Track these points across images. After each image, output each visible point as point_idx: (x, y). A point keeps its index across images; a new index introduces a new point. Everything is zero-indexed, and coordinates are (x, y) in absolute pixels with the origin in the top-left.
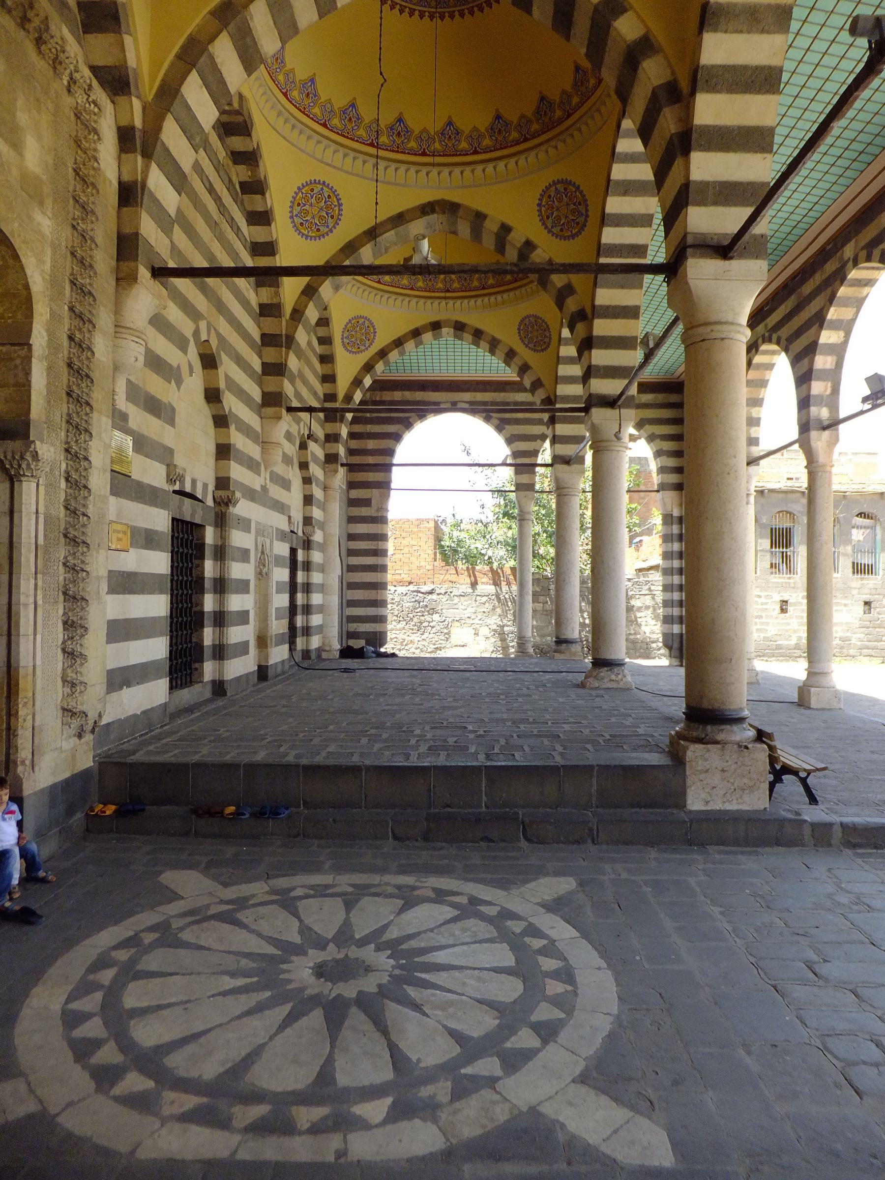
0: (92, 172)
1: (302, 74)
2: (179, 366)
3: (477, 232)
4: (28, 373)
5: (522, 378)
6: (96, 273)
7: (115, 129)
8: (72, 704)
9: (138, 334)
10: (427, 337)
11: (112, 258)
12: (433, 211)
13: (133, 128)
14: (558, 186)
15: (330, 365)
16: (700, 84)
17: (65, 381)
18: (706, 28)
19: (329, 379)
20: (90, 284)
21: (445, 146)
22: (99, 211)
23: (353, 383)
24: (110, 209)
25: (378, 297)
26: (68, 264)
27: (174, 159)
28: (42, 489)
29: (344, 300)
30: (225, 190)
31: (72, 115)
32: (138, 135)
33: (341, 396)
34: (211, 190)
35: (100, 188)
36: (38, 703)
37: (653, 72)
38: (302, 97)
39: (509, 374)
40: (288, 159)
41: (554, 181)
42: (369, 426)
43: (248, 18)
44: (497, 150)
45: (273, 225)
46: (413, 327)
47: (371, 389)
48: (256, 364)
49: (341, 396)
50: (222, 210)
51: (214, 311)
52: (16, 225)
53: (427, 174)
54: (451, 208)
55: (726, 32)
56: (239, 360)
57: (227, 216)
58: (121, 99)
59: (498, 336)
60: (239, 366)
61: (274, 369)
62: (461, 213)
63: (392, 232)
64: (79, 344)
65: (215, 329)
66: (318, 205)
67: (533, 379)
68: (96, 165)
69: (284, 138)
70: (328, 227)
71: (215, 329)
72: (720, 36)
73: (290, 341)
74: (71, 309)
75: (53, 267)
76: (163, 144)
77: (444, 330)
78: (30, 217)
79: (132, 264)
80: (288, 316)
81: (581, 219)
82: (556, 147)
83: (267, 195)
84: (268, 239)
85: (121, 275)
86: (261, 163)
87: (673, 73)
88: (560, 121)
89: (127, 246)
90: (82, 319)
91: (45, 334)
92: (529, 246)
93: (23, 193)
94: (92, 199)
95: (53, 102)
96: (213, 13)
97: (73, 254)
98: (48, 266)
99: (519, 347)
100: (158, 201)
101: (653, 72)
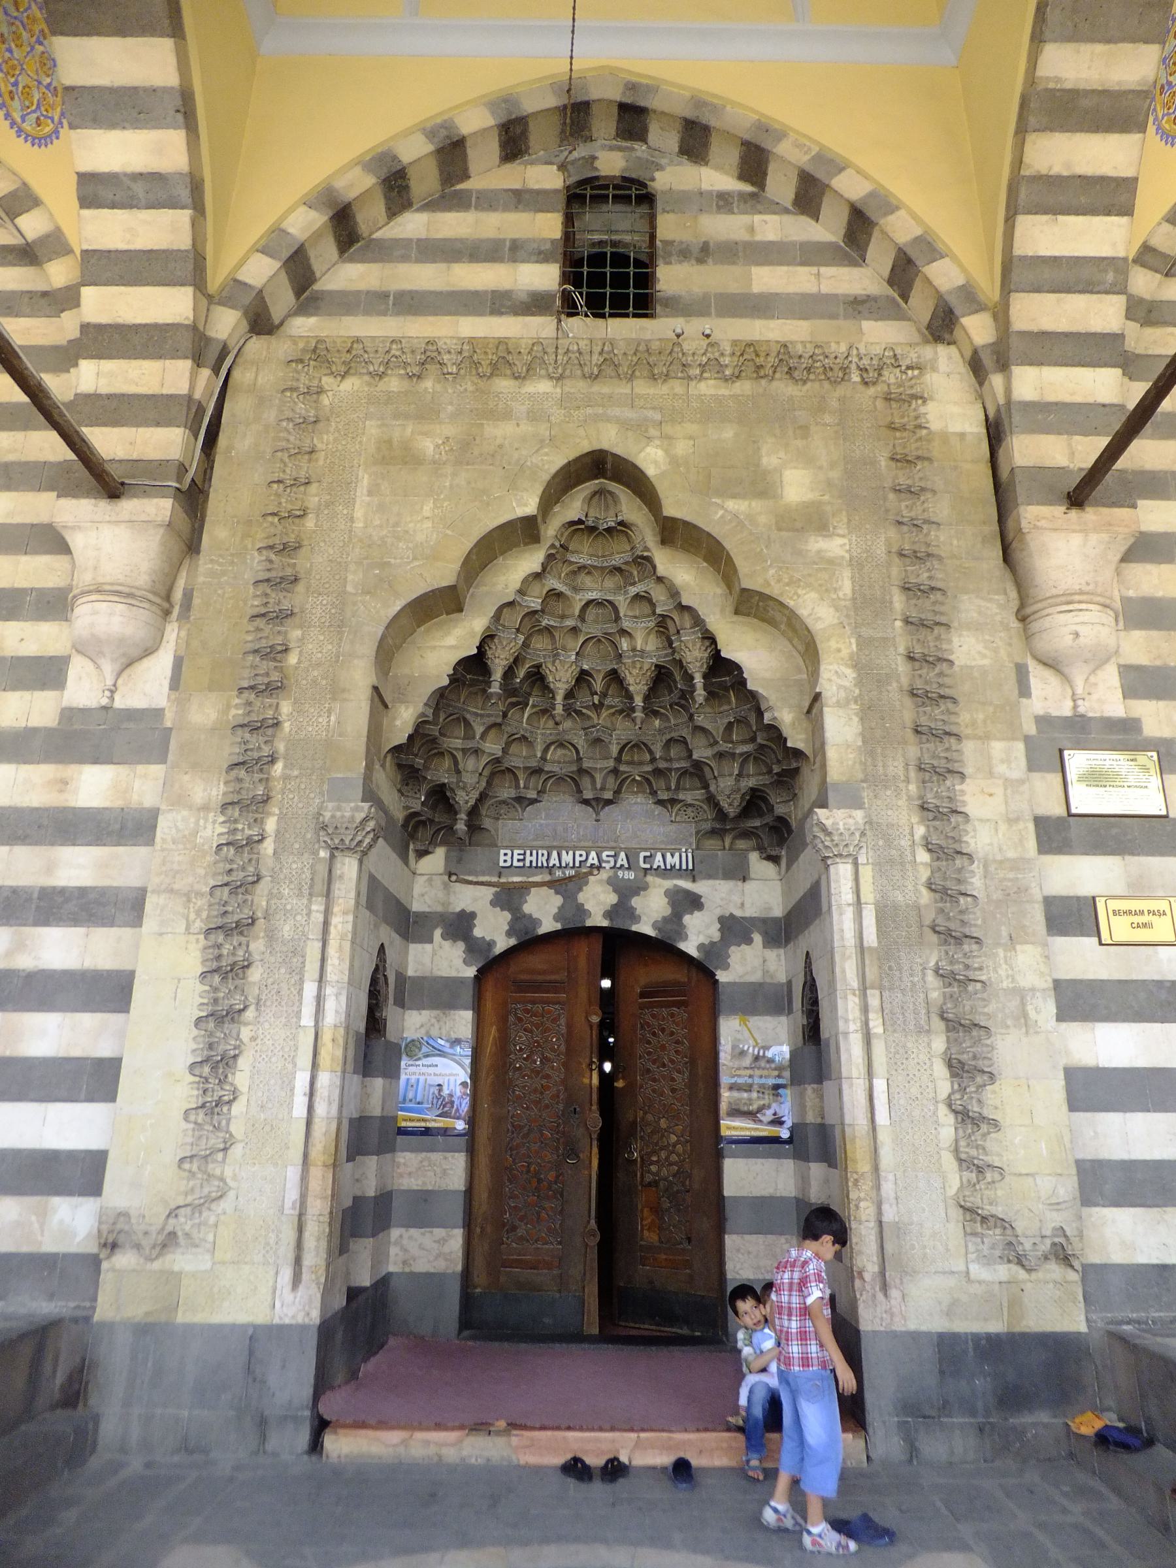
8: (974, 1200)
9: (1063, 599)
20: (930, 578)
28: (866, 873)
36: (888, 1188)
43: (1051, 85)
68: (924, 432)
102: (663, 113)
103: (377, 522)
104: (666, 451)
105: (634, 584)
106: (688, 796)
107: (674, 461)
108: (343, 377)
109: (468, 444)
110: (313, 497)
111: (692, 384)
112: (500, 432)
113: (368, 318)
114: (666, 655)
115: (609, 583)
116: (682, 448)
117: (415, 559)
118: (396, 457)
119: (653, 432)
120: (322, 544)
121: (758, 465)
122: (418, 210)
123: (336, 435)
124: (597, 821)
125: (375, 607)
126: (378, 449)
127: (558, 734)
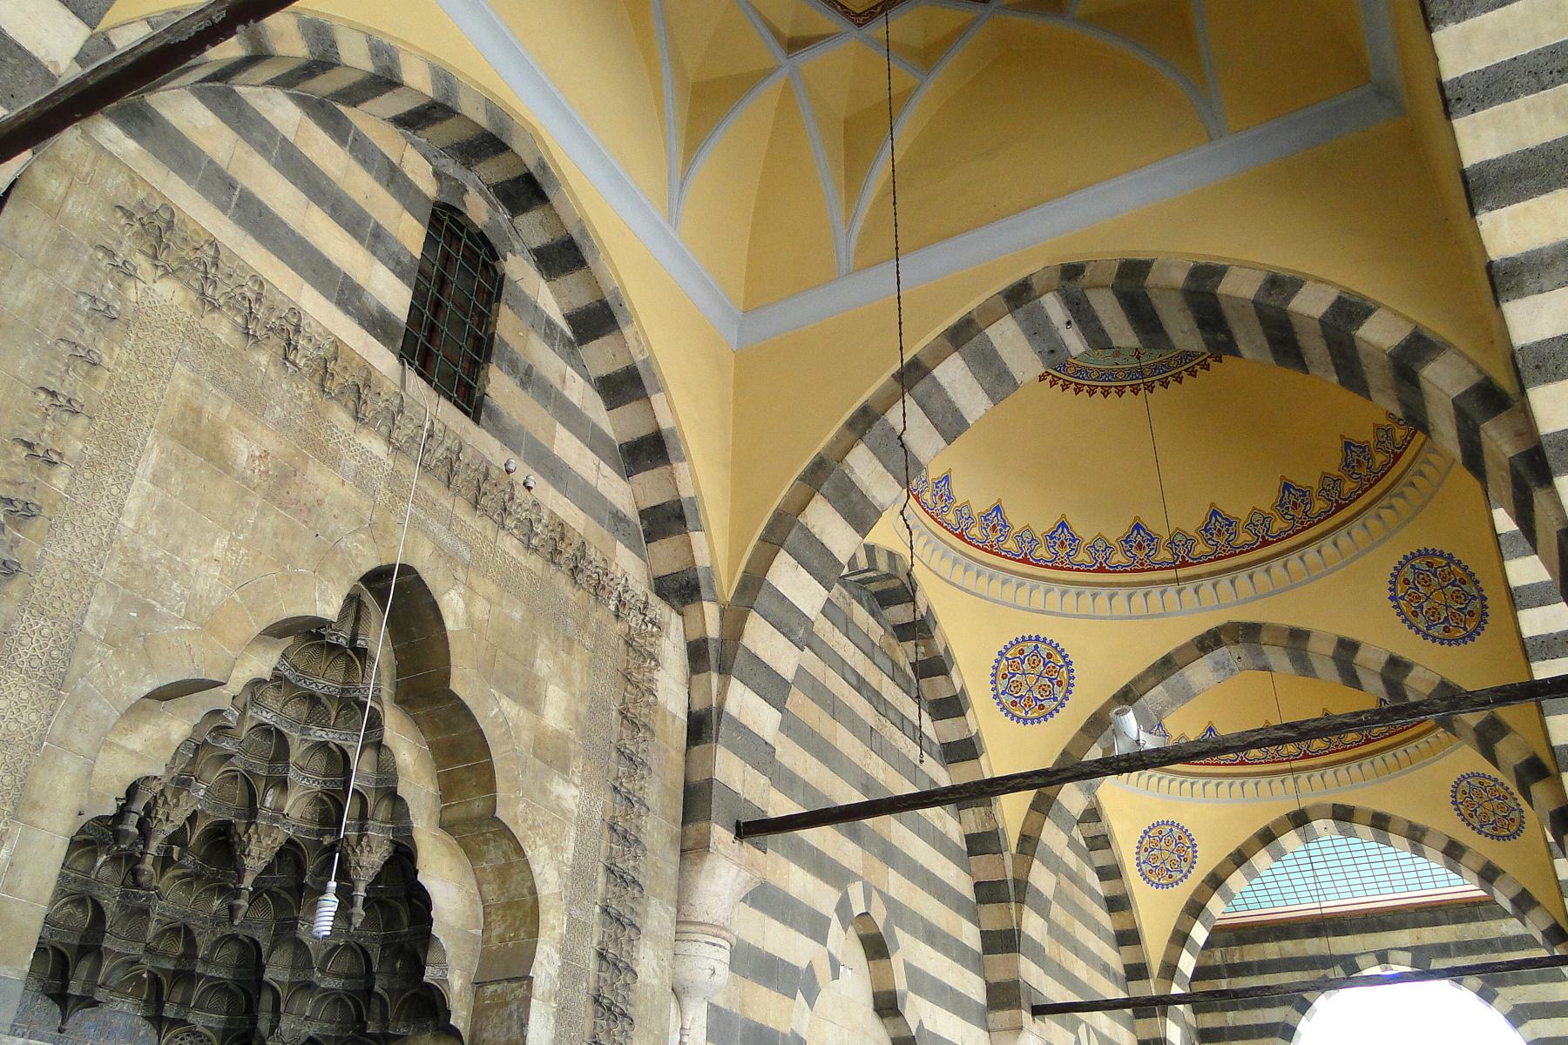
0: (645, 711)
1: (980, 505)
2: (810, 966)
3: (1302, 664)
4: (523, 1024)
5: (1490, 892)
6: (644, 850)
7: (683, 647)
9: (715, 931)
10: (1290, 840)
11: (675, 821)
12: (1218, 643)
13: (705, 640)
14: (1416, 562)
15: (1126, 913)
16: (1526, 375)
17: (588, 1026)
18: (1501, 295)
19: (1128, 937)
21: (1222, 543)
22: (652, 760)
23: (1172, 940)
24: (673, 753)
25: (1187, 785)
26: (604, 844)
27: (767, 667)
29: (1128, 804)
30: (886, 680)
31: (621, 642)
32: (712, 647)
33: (1155, 967)
34: (861, 685)
35: (656, 728)
37: (1444, 380)
38: (988, 535)
39: (1461, 886)
40: (975, 621)
41: (1405, 557)
42: (1230, 1014)
44: (1299, 532)
45: (969, 713)
46: (1259, 826)
47: (1208, 944)
48: (970, 936)
49: (1155, 967)
50: (882, 709)
51: (877, 864)
52: (522, 806)
53: (1196, 591)
54: (1248, 633)
55: (1540, 292)
56: (933, 936)
57: (892, 716)
58: (691, 609)
59: (1419, 820)
60: (932, 944)
61: (1003, 941)
62: (1264, 637)
63: (1160, 688)
64: (615, 963)
65: (880, 892)
66: (1035, 674)
67: (1514, 891)
69: (967, 591)
70: (1055, 699)
71: (880, 892)
72: (1530, 300)
73: (1021, 891)
74: (605, 910)
75: (578, 853)
76: (747, 650)
77: (1319, 825)
78: (544, 791)
79: (703, 825)
80: (1014, 850)
81: (1475, 605)
82: (1391, 507)
83: (953, 673)
84: (966, 735)
85: (690, 844)
86: (937, 633)
87: (1480, 371)
88: (1387, 468)
89: (696, 799)
90: (620, 923)
91: (556, 957)
92: (1396, 667)
93: (538, 761)
94: (643, 746)
95: (591, 635)
96: (801, 479)
97: (612, 828)
98: (569, 855)
99: (1465, 835)
100: (745, 727)
101: (1444, 380)
102: (557, 216)
103: (153, 532)
104: (467, 605)
105: (323, 726)
106: (198, 1020)
107: (470, 621)
108: (166, 273)
109: (286, 476)
110: (76, 441)
111: (502, 533)
112: (324, 481)
113: (202, 199)
114: (308, 832)
115: (292, 710)
116: (480, 609)
117: (187, 618)
118: (198, 441)
119: (460, 574)
120: (68, 528)
121: (532, 666)
122: (293, 97)
123: (133, 357)
124: (60, 1031)
125: (116, 674)
126: (182, 416)
127: (86, 883)
